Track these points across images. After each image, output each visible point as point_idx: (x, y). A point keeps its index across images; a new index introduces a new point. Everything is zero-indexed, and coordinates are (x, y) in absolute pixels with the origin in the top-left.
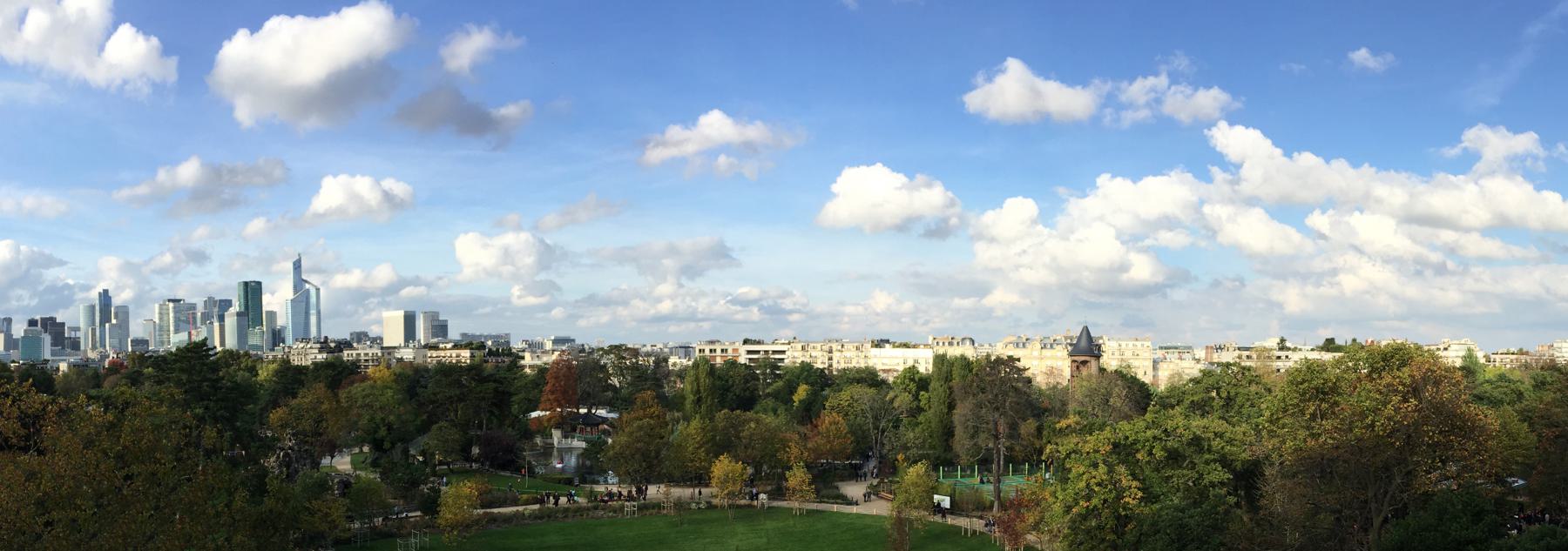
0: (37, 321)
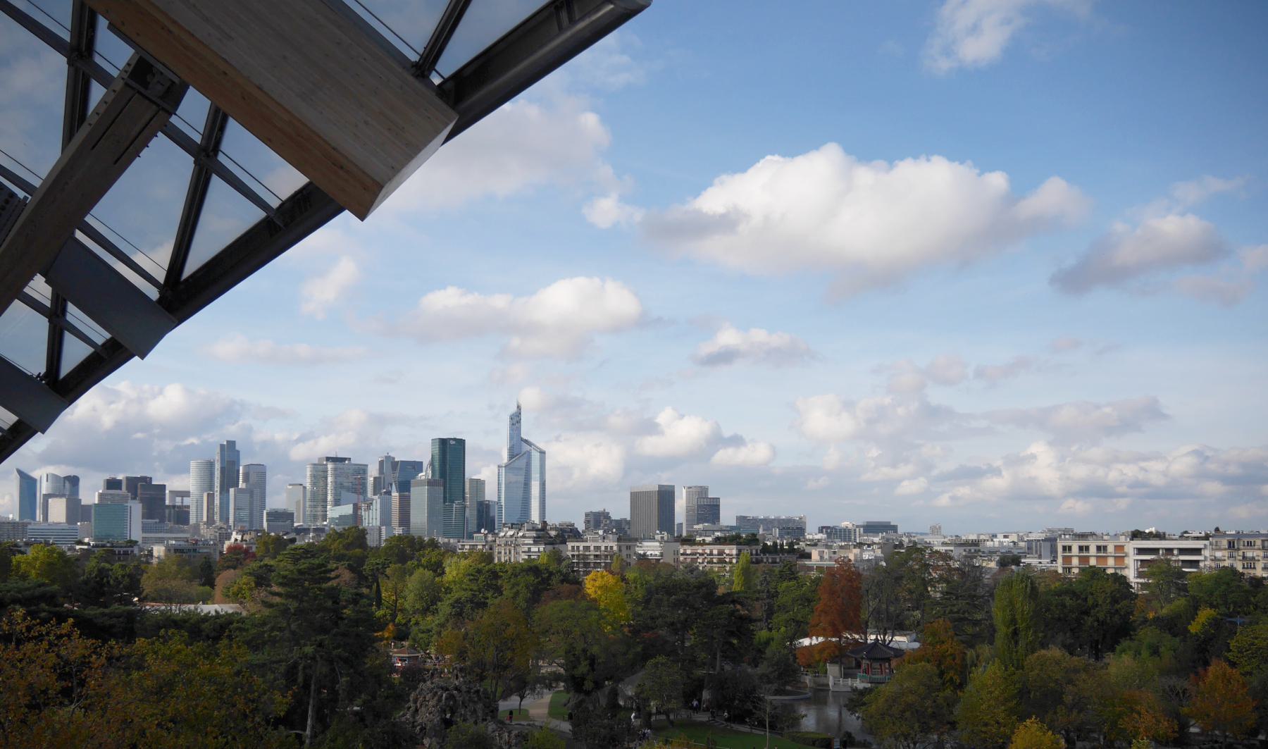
0: (120, 481)
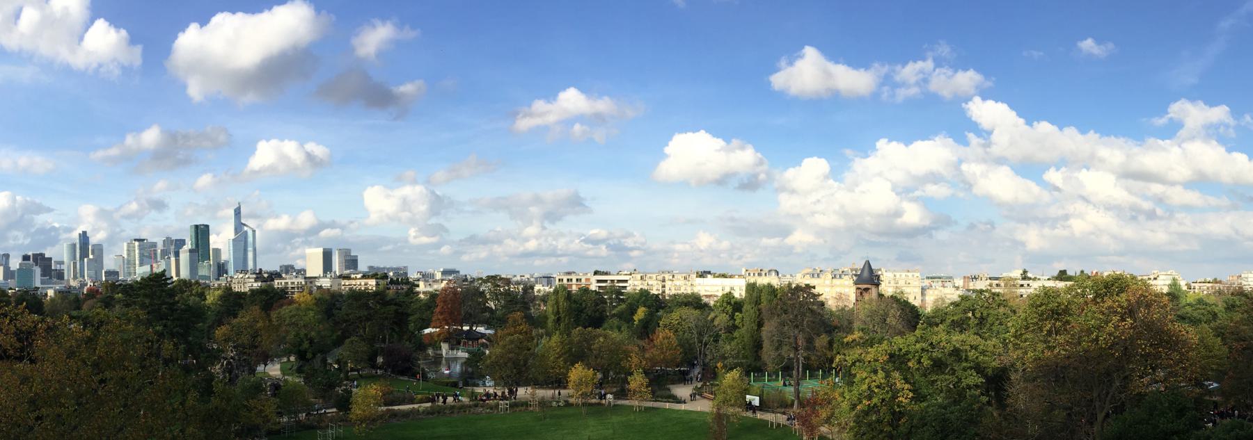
0: (29, 256)
